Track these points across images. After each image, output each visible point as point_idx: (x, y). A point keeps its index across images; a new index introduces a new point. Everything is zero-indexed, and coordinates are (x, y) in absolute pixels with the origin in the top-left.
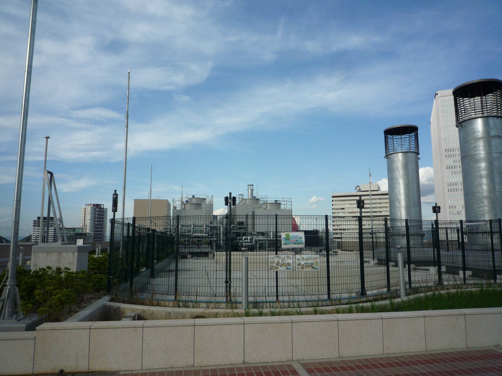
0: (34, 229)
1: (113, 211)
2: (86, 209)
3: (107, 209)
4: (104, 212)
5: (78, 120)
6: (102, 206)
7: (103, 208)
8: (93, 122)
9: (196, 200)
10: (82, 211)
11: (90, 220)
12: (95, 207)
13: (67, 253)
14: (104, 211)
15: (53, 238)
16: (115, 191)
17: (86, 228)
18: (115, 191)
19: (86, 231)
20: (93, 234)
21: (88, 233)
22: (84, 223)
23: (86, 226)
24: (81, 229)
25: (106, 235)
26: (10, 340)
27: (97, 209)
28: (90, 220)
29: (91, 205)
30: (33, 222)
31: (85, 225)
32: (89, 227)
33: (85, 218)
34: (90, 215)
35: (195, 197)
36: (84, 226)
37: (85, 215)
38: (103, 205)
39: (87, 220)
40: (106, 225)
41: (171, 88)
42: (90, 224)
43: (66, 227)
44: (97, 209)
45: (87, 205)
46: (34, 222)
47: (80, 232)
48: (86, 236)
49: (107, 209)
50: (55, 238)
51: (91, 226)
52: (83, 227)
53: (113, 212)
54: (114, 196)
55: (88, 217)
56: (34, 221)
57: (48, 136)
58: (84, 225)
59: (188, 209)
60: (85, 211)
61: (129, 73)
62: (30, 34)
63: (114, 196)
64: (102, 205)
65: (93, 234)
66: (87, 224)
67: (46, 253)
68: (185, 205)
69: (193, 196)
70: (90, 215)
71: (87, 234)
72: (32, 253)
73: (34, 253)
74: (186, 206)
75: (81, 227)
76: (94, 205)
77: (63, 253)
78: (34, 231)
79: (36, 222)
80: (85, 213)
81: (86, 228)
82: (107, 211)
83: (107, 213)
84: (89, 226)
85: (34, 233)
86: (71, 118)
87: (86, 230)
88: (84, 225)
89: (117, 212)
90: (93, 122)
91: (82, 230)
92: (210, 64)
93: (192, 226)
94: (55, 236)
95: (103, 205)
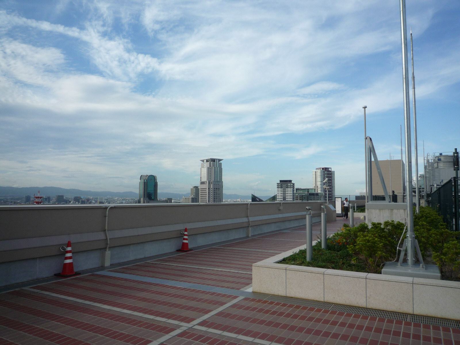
0: (278, 190)
1: (454, 170)
2: (317, 172)
3: (334, 171)
4: (332, 175)
5: (304, 96)
6: (330, 169)
7: (331, 171)
8: (316, 96)
9: (445, 158)
10: (313, 174)
11: (320, 181)
12: (324, 171)
13: (398, 210)
14: (332, 173)
15: (283, 198)
16: (456, 149)
17: (318, 189)
18: (456, 149)
19: (318, 192)
20: (324, 194)
21: (320, 193)
22: (316, 184)
23: (318, 187)
24: (313, 190)
25: (335, 195)
26: (440, 286)
27: (326, 172)
28: (320, 181)
29: (320, 168)
30: (277, 185)
31: (316, 186)
32: (320, 188)
33: (316, 180)
34: (320, 177)
35: (443, 154)
36: (316, 187)
37: (316, 177)
38: (331, 168)
39: (317, 182)
40: (334, 186)
41: (387, 48)
42: (321, 185)
43: (302, 188)
44: (325, 172)
45: (317, 169)
46: (277, 185)
47: (313, 192)
48: (318, 196)
49: (334, 171)
50: (293, 197)
51: (322, 187)
52: (315, 188)
53: (455, 171)
54: (455, 155)
55: (319, 179)
56: (277, 183)
57: (366, 106)
58: (316, 186)
59: (441, 168)
60: (316, 174)
61: (411, 34)
62: (401, 9)
63: (455, 155)
64: (330, 168)
65: (324, 194)
66: (318, 185)
67: (379, 209)
68: (438, 164)
69: (441, 154)
70: (320, 177)
71: (319, 194)
72: (366, 209)
73: (368, 209)
74: (439, 164)
75: (314, 188)
76: (323, 169)
77: (395, 210)
78: (278, 192)
79: (279, 185)
80: (316, 176)
81: (318, 189)
82: (334, 173)
83: (334, 175)
84: (320, 187)
85: (278, 194)
86: (298, 96)
87: (318, 190)
88: (316, 186)
89: (459, 170)
90: (316, 96)
91: (314, 190)
92: (431, 12)
93: (435, 185)
94: (293, 195)
95: (331, 168)
